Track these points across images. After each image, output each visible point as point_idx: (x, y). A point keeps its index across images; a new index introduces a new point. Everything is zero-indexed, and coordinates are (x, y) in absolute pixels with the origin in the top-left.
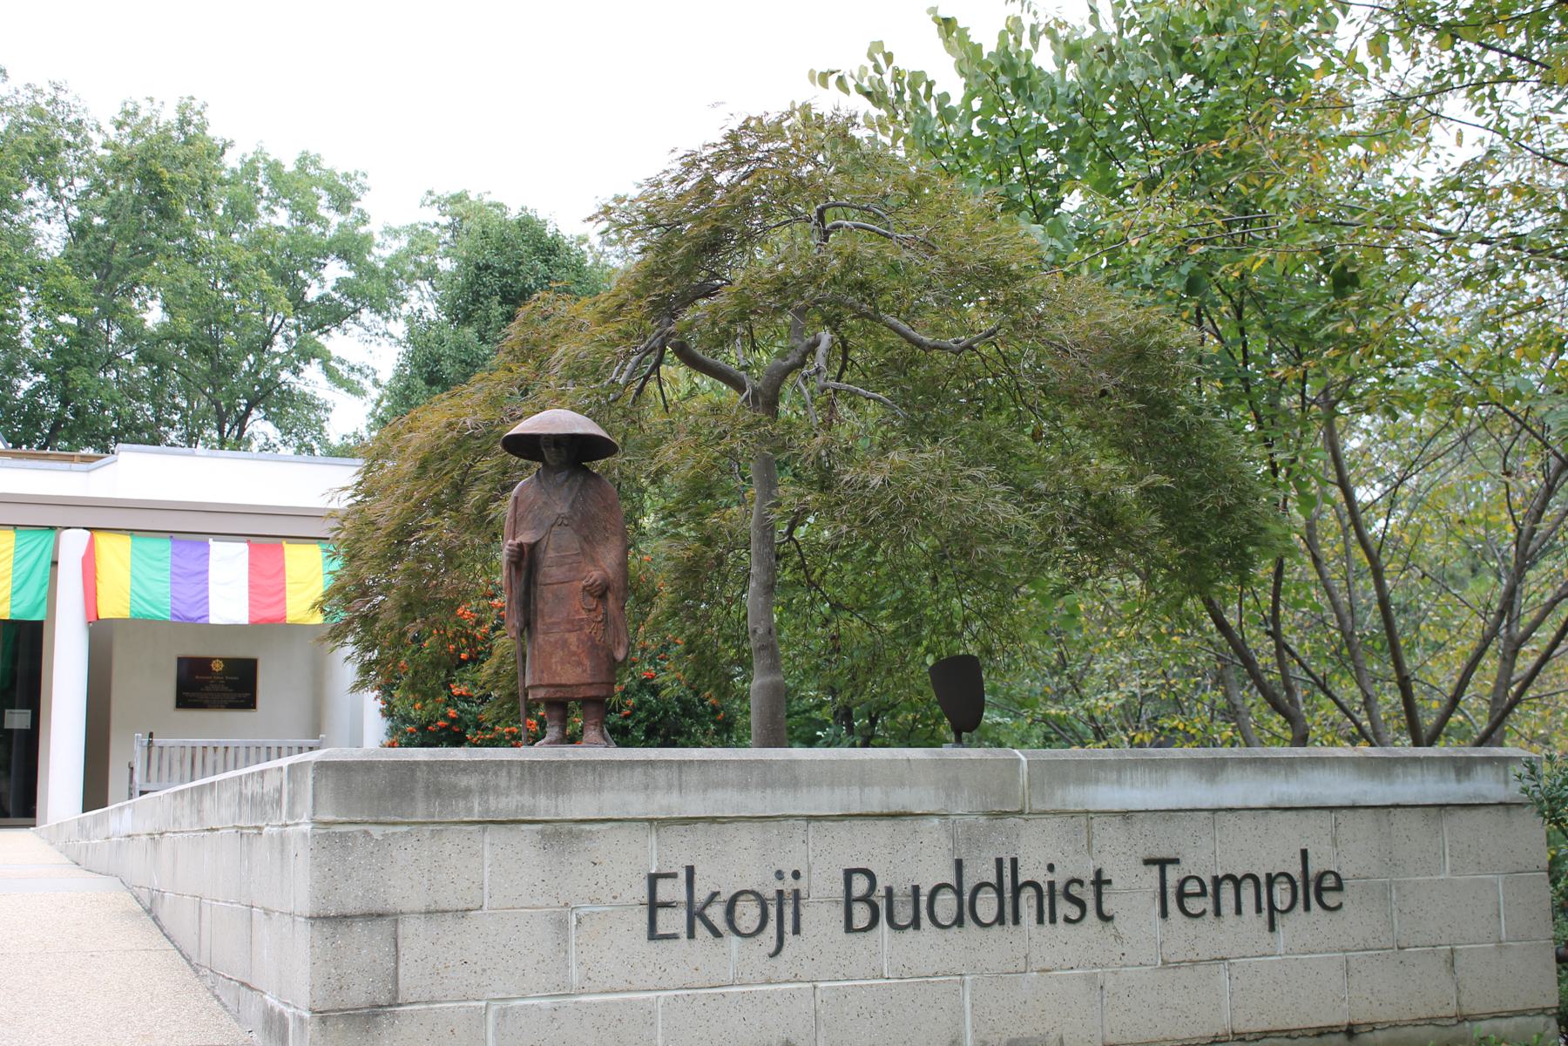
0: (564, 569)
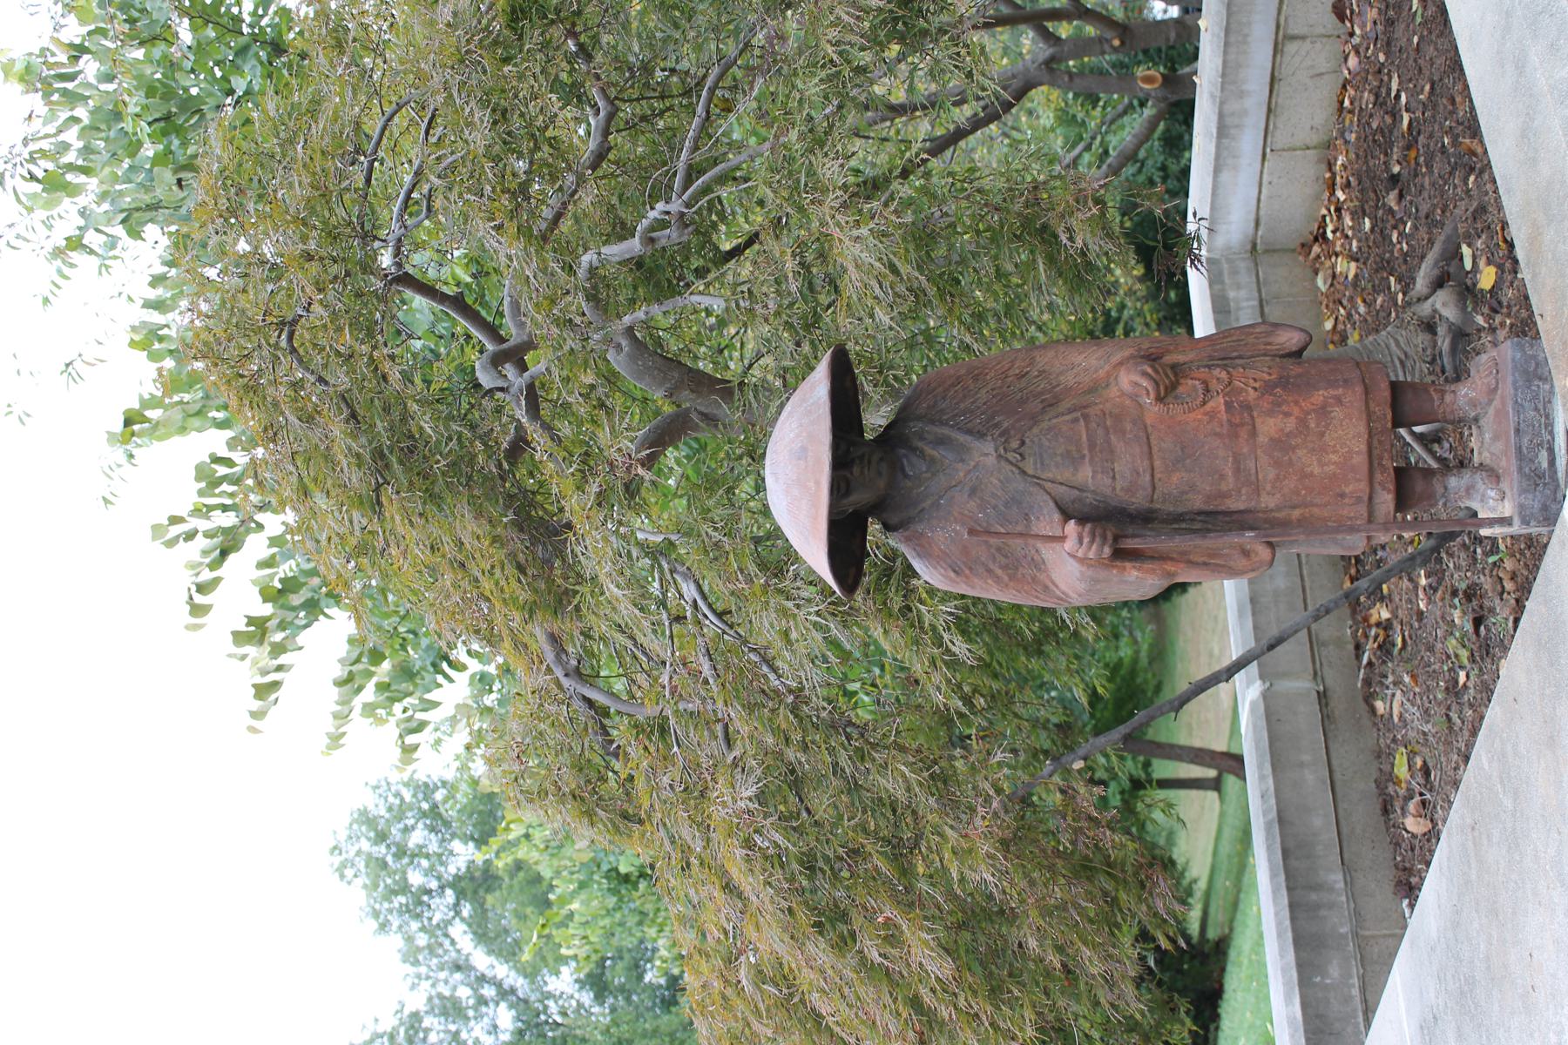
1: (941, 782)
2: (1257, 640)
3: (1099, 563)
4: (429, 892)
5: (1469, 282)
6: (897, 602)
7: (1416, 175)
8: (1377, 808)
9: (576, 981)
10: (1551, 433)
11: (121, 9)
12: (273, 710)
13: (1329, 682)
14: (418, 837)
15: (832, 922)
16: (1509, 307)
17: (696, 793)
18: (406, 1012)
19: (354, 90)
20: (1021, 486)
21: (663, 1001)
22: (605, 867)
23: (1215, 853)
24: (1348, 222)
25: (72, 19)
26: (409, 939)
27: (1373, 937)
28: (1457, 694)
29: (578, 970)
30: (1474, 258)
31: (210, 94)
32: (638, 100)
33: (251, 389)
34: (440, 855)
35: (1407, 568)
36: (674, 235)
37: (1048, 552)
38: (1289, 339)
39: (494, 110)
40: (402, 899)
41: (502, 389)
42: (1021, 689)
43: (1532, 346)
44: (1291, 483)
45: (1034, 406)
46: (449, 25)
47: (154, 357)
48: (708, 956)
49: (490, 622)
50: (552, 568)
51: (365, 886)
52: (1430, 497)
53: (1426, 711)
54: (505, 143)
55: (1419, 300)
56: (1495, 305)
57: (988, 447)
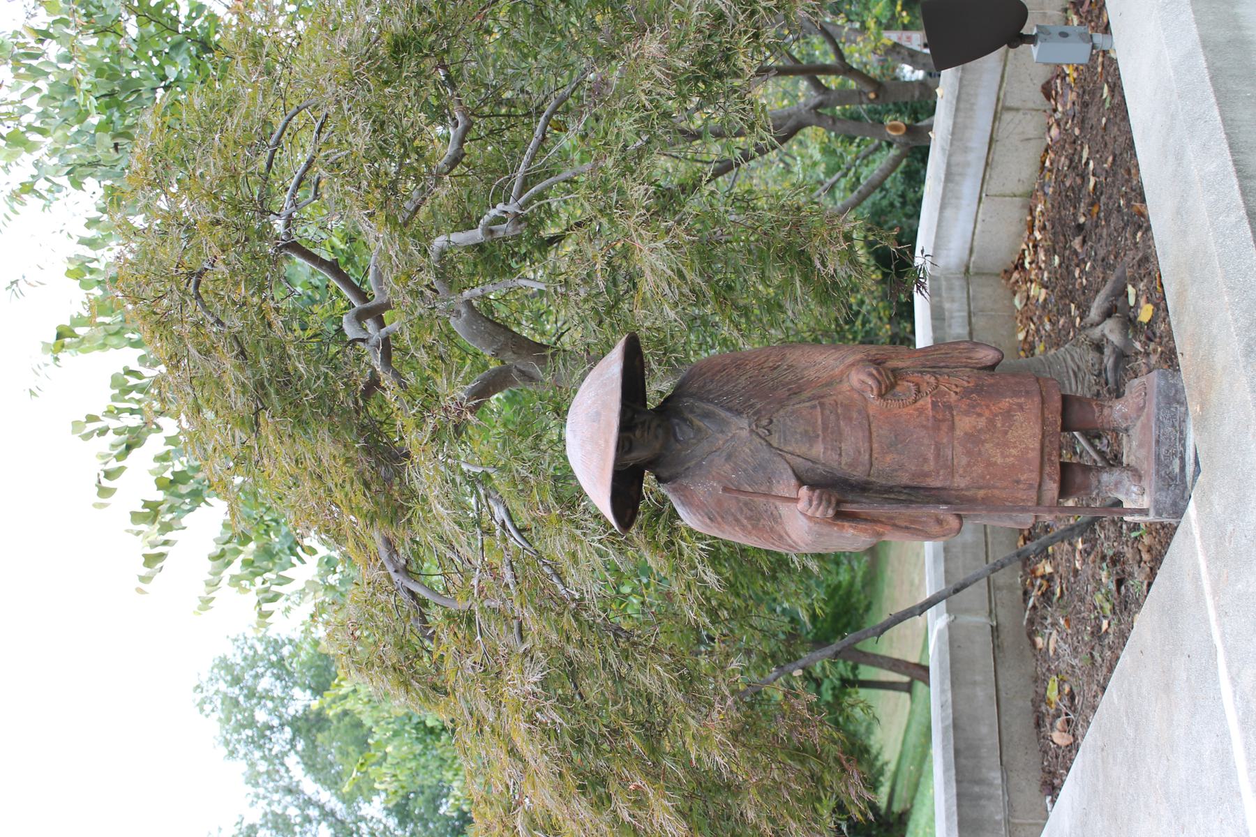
0: (846, 430)
1: (688, 681)
2: (947, 582)
3: (824, 521)
4: (271, 728)
5: (1131, 315)
6: (663, 538)
7: (1097, 227)
8: (1032, 722)
9: (385, 809)
10: (1184, 446)
11: (81, 5)
12: (158, 576)
13: (1001, 619)
14: (266, 683)
15: (593, 785)
16: (1161, 337)
17: (492, 674)
18: (245, 824)
19: (264, 96)
20: (767, 456)
21: (454, 829)
22: (415, 720)
23: (904, 742)
24: (1042, 256)
25: (42, 11)
26: (252, 765)
27: (1021, 824)
28: (1099, 638)
29: (387, 801)
30: (1137, 296)
31: (147, 78)
32: (489, 116)
33: (162, 324)
34: (282, 699)
35: (1069, 534)
36: (510, 229)
37: (784, 509)
38: (986, 356)
39: (374, 121)
40: (249, 732)
41: (363, 340)
42: (758, 606)
43: (1173, 376)
44: (978, 469)
45: (782, 393)
46: (344, 51)
47: (85, 285)
48: (491, 804)
49: (339, 525)
50: (391, 486)
51: (220, 720)
52: (1086, 487)
53: (1075, 649)
54: (381, 148)
55: (1092, 325)
56: (1150, 335)
57: (744, 423)
